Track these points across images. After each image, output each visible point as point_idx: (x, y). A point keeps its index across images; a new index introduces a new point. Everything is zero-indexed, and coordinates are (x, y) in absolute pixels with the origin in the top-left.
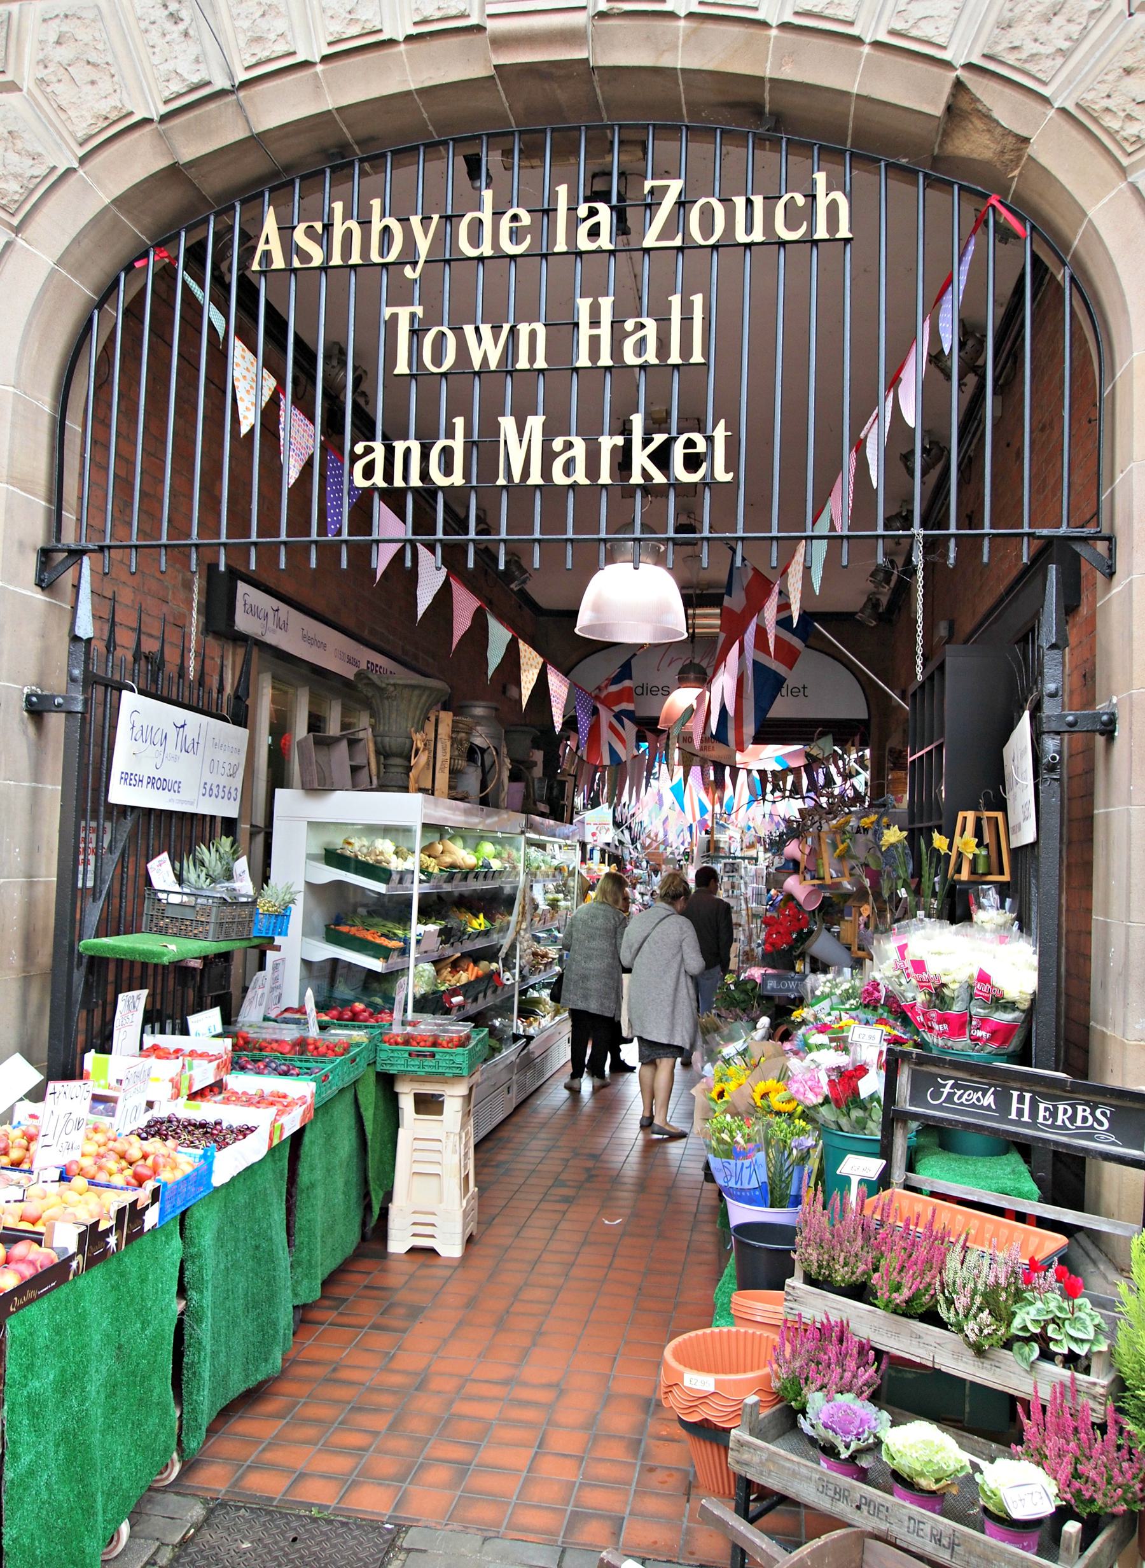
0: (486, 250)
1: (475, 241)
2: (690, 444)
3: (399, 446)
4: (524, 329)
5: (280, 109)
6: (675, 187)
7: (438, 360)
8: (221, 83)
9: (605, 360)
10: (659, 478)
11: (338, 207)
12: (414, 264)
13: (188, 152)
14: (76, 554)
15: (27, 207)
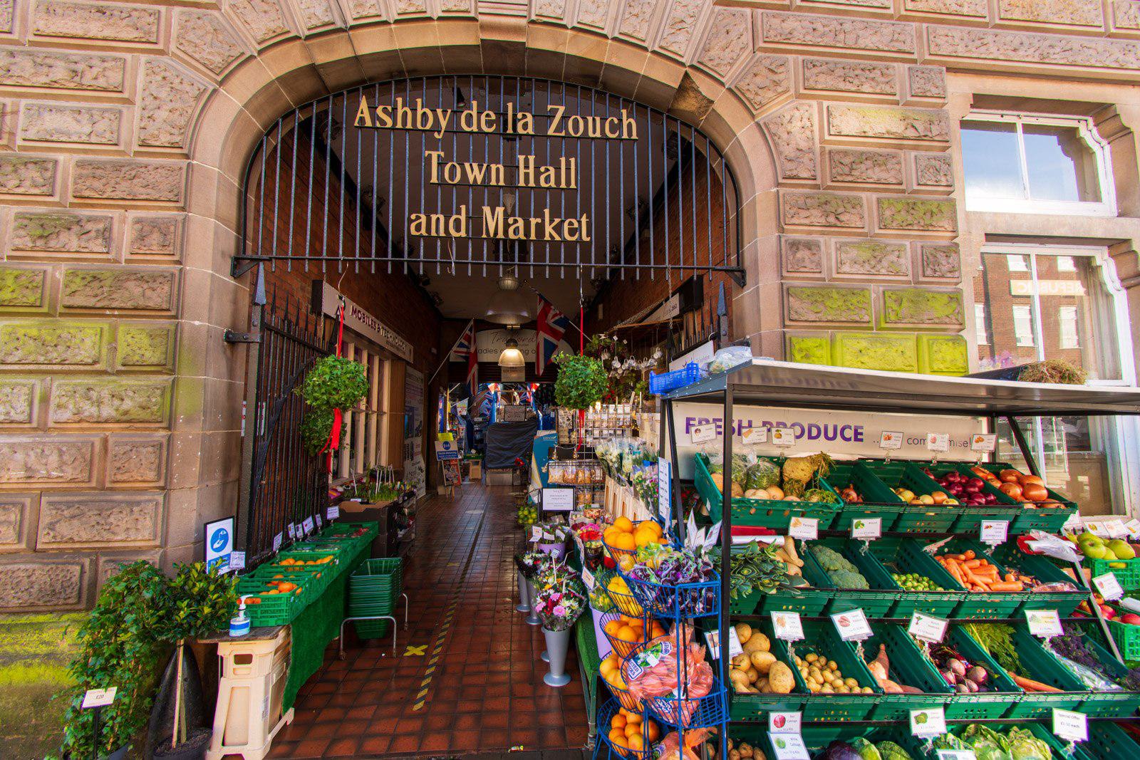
0: (475, 128)
1: (469, 123)
2: (571, 224)
3: (434, 217)
4: (494, 167)
5: (371, 44)
6: (562, 109)
7: (452, 178)
8: (339, 24)
9: (532, 184)
10: (557, 238)
11: (400, 100)
12: (439, 132)
13: (321, 59)
14: (257, 261)
15: (227, 72)
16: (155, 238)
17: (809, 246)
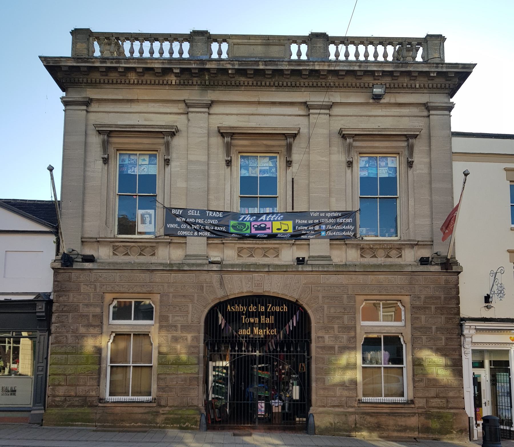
16: (195, 340)
17: (321, 337)
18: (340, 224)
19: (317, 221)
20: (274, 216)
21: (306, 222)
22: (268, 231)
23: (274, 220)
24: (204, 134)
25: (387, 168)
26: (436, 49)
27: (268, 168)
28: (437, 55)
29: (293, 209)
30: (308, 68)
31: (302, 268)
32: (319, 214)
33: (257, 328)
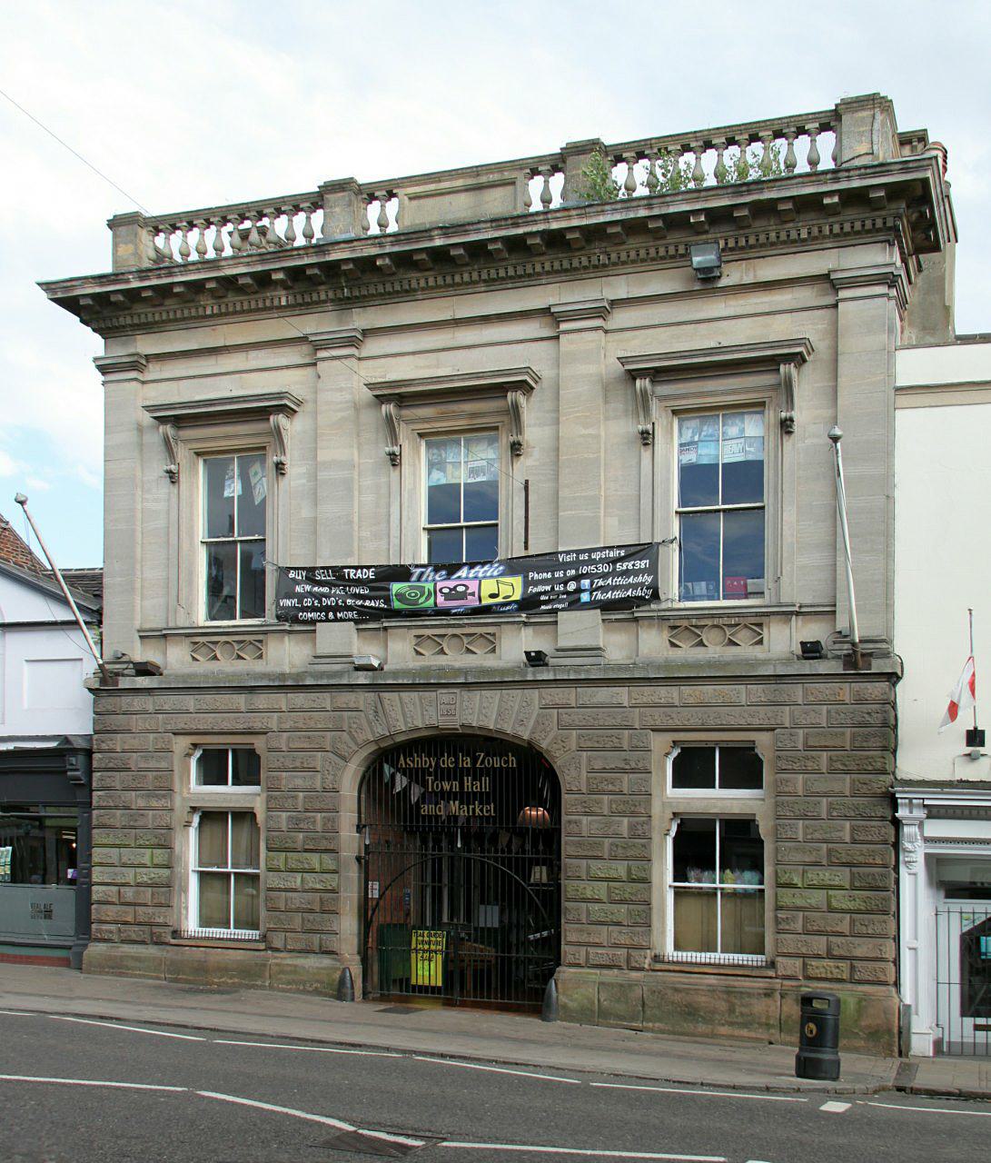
18: (626, 573)
19: (573, 572)
20: (486, 568)
21: (549, 575)
22: (472, 602)
23: (485, 577)
24: (346, 402)
25: (742, 440)
26: (861, 134)
27: (484, 463)
28: (863, 148)
29: (526, 548)
30: (535, 229)
31: (534, 674)
32: (577, 558)
33: (457, 802)
